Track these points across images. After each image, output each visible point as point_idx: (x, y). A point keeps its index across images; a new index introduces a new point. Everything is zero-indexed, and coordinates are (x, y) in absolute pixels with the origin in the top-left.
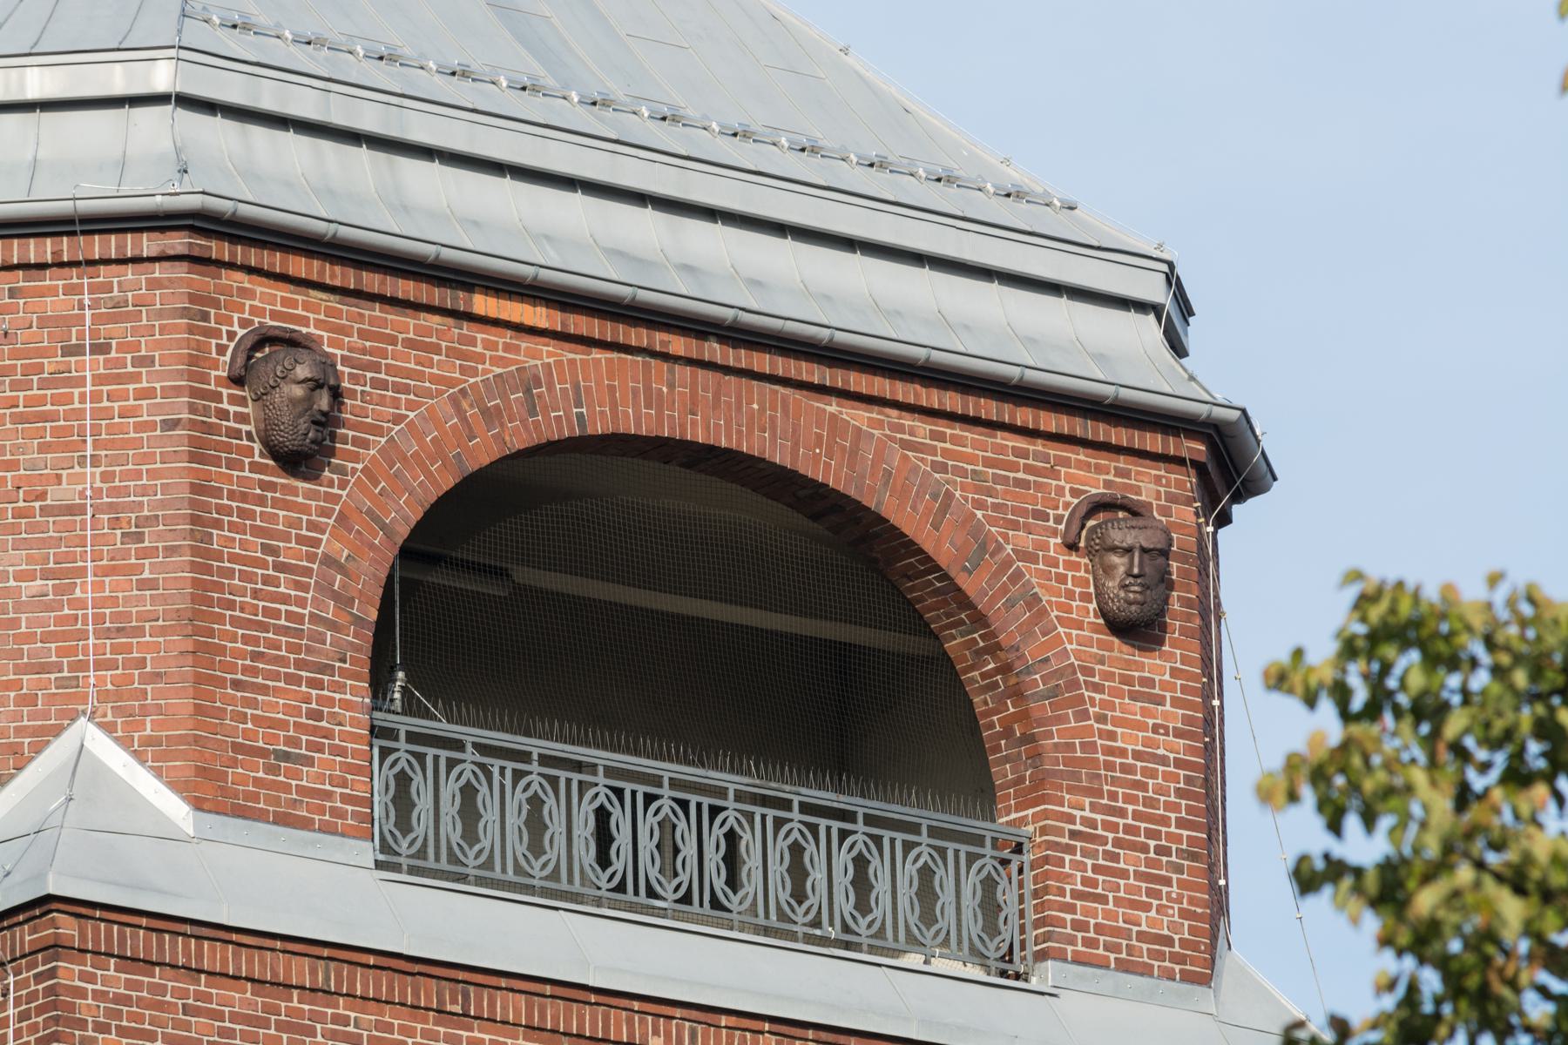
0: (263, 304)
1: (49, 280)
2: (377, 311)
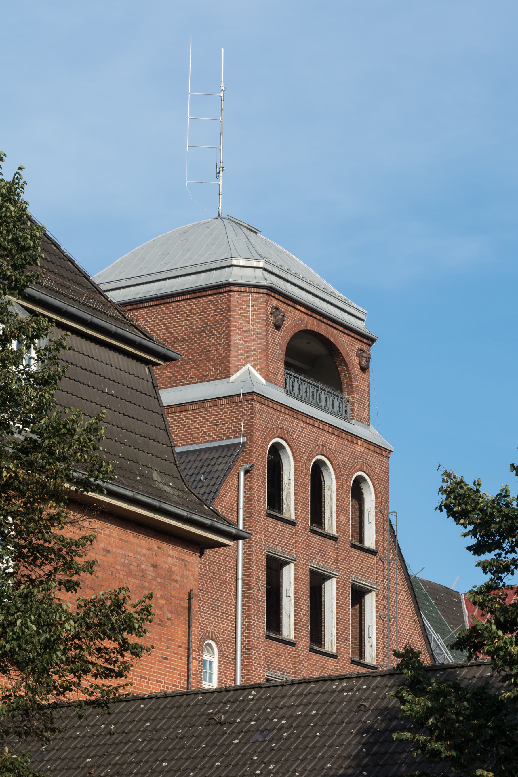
0: (274, 302)
1: (244, 294)
2: (286, 306)
